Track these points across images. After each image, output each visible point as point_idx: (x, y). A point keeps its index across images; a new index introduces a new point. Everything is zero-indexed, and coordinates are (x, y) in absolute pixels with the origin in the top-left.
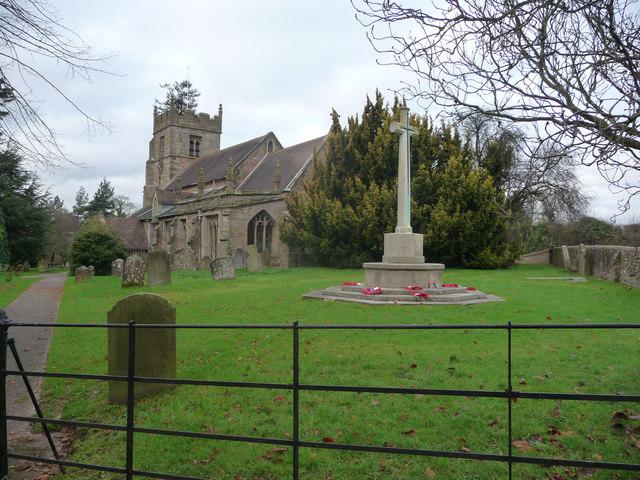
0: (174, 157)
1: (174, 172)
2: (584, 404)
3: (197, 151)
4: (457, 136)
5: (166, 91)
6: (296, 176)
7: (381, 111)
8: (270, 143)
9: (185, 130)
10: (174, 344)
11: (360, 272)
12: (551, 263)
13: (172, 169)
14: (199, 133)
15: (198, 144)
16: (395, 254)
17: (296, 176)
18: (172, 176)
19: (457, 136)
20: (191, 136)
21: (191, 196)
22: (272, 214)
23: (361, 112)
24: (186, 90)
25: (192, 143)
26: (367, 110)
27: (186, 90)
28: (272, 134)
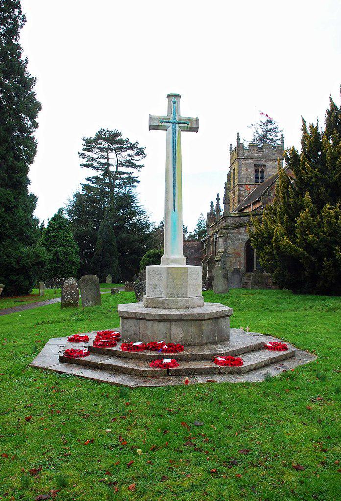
0: (241, 186)
1: (242, 198)
3: (262, 178)
5: (253, 130)
9: (250, 161)
10: (301, 296)
11: (26, 301)
13: (239, 196)
14: (263, 162)
15: (262, 171)
18: (239, 202)
20: (255, 166)
24: (270, 126)
25: (257, 171)
27: (270, 126)
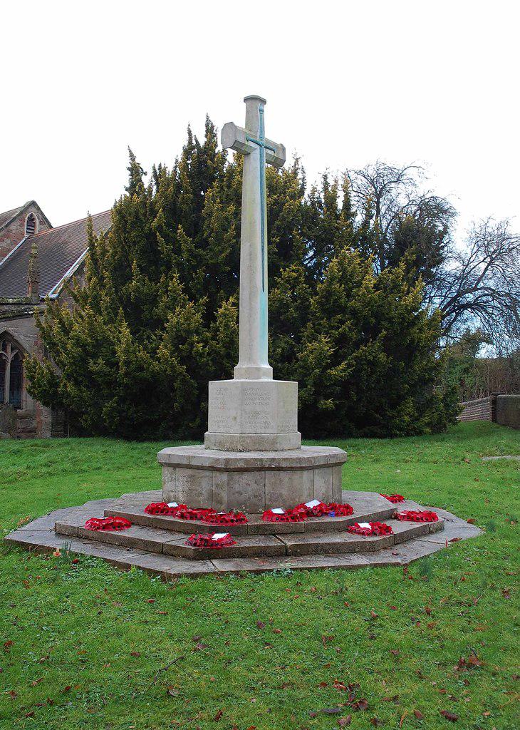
2: (243, 290)
4: (347, 204)
6: (68, 274)
7: (213, 156)
8: (31, 219)
12: (494, 419)
16: (235, 430)
17: (68, 274)
19: (347, 204)
21: (499, 303)
22: (21, 339)
23: (179, 153)
26: (187, 153)
28: (33, 204)
